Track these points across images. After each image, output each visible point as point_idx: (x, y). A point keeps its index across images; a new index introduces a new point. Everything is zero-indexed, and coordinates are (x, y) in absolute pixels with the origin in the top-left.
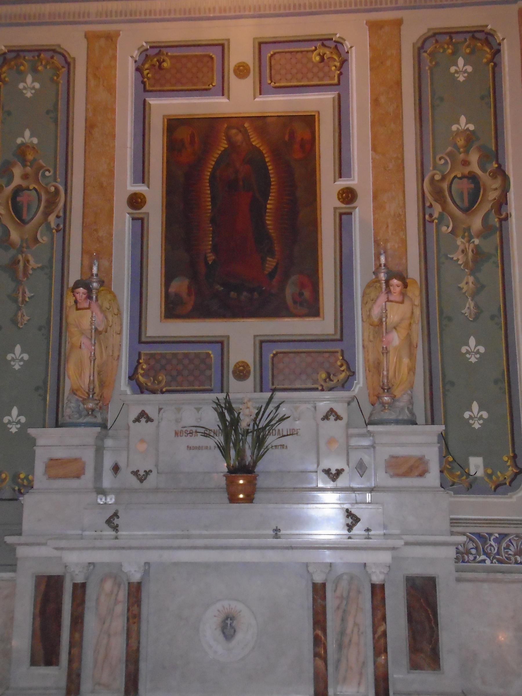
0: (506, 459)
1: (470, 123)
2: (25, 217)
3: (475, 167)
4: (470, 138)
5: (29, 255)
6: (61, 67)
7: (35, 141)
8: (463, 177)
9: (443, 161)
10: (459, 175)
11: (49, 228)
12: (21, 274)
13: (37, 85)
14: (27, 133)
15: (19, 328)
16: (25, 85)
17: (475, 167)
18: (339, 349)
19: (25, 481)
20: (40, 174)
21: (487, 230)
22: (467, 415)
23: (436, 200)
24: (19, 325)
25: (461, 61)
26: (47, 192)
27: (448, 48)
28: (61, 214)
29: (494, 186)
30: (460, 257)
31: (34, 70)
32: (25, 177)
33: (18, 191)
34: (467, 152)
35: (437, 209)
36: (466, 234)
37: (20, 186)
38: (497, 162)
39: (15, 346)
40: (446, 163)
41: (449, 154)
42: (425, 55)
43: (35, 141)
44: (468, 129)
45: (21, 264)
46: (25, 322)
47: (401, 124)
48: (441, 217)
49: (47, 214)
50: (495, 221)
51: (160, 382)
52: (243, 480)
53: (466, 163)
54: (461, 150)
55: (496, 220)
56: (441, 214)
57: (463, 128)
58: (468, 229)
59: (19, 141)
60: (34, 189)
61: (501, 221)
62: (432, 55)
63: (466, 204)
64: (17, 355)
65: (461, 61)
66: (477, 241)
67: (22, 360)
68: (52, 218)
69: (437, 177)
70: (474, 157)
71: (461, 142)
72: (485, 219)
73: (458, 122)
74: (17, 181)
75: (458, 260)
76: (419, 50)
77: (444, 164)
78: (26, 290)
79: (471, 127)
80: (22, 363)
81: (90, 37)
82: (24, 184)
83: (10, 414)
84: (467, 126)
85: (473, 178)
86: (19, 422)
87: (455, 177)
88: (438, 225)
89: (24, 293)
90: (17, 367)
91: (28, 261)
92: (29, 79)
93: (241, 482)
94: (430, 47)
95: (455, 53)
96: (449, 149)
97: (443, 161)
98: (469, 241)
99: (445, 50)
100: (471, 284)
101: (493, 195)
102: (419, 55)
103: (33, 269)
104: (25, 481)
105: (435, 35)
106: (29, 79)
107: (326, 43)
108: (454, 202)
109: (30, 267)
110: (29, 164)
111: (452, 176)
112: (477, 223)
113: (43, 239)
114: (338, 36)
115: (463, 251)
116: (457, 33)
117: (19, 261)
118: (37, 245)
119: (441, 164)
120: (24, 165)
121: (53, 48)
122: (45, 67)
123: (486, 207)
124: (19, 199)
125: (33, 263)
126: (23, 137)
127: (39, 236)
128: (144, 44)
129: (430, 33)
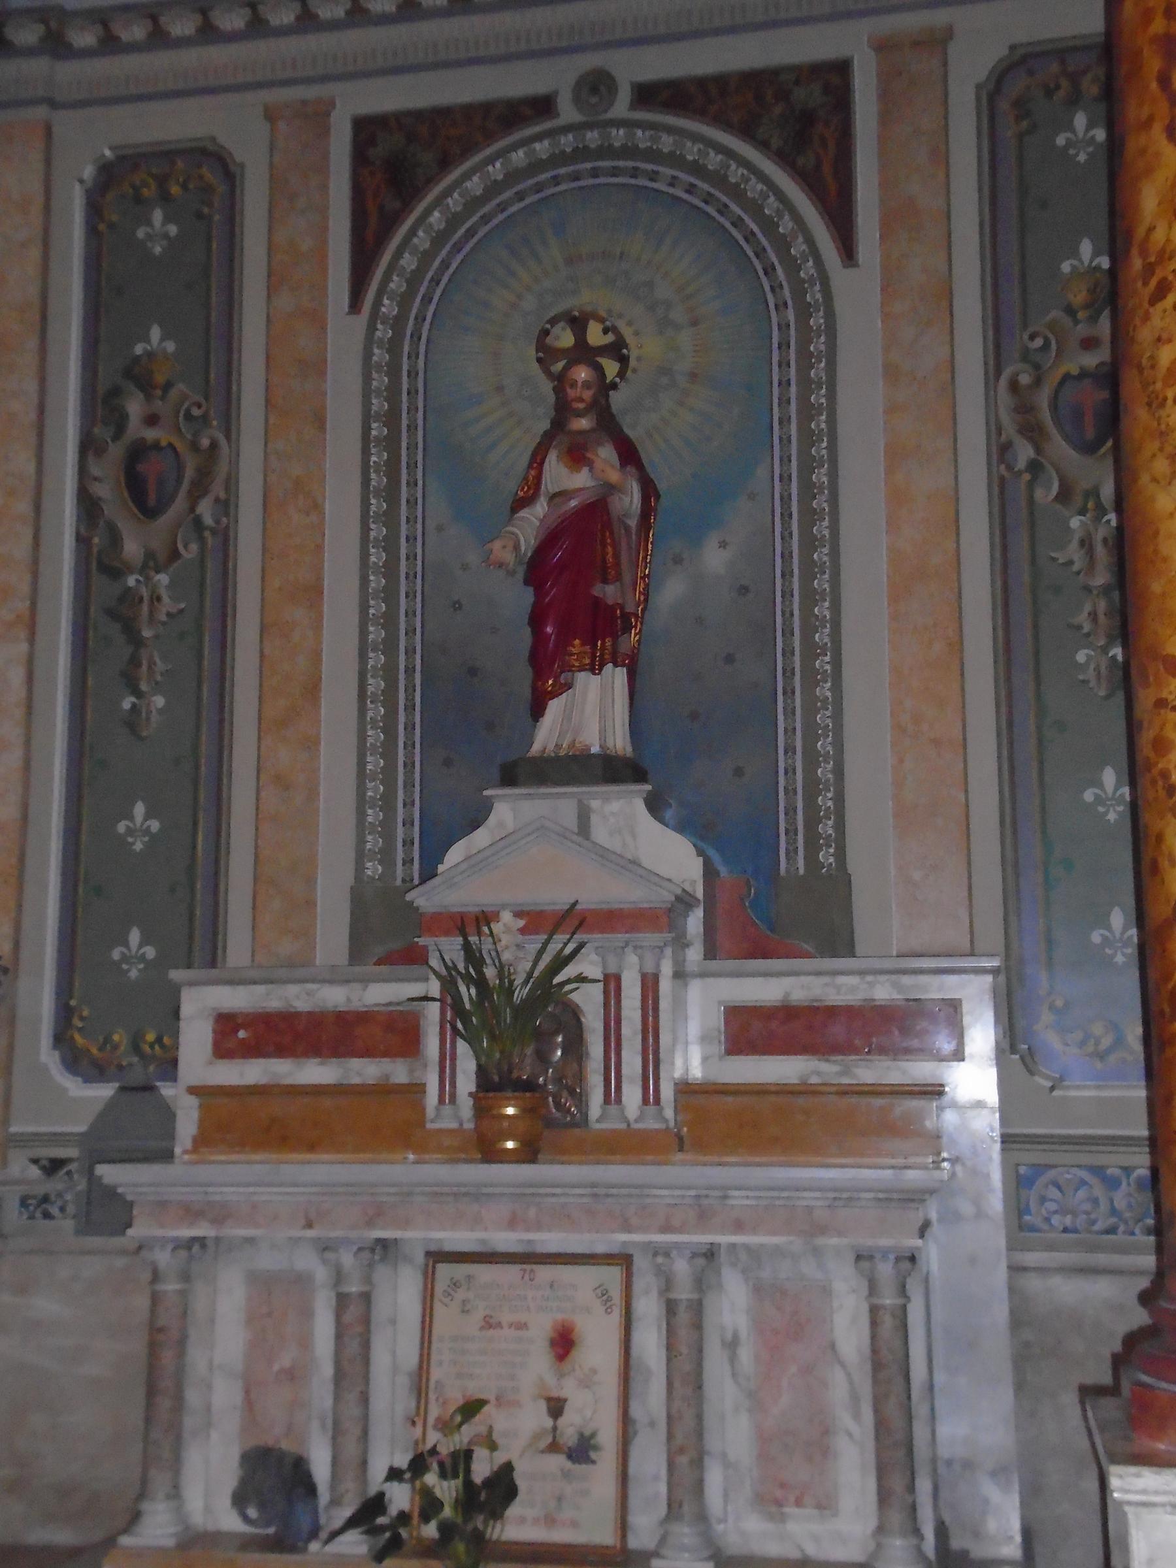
2: (152, 501)
5: (156, 654)
6: (192, 516)
7: (170, 346)
9: (1039, 342)
10: (1075, 371)
11: (198, 523)
13: (173, 230)
14: (155, 333)
16: (149, 230)
18: (554, 77)
19: (157, 1047)
25: (1080, 120)
26: (194, 446)
28: (222, 495)
30: (1076, 558)
31: (165, 198)
32: (152, 420)
35: (1024, 453)
36: (1090, 505)
39: (128, 933)
40: (1046, 346)
43: (170, 346)
48: (1035, 467)
51: (116, 1047)
54: (1081, 315)
59: (139, 349)
60: (170, 445)
65: (1080, 120)
67: (166, 236)
68: (205, 509)
69: (1025, 379)
73: (1075, 253)
75: (1071, 563)
76: (993, 91)
82: (151, 434)
86: (147, 831)
88: (1031, 485)
89: (152, 664)
91: (159, 599)
92: (158, 216)
93: (510, 1111)
94: (1017, 85)
97: (1039, 342)
98: (1097, 519)
100: (1102, 619)
103: (168, 614)
104: (157, 1047)
106: (158, 216)
110: (159, 392)
113: (190, 552)
115: (1082, 543)
116: (1075, 49)
119: (1036, 350)
120: (149, 397)
122: (184, 187)
124: (140, 467)
125: (168, 604)
126: (148, 342)
127: (180, 547)
128: (108, 153)
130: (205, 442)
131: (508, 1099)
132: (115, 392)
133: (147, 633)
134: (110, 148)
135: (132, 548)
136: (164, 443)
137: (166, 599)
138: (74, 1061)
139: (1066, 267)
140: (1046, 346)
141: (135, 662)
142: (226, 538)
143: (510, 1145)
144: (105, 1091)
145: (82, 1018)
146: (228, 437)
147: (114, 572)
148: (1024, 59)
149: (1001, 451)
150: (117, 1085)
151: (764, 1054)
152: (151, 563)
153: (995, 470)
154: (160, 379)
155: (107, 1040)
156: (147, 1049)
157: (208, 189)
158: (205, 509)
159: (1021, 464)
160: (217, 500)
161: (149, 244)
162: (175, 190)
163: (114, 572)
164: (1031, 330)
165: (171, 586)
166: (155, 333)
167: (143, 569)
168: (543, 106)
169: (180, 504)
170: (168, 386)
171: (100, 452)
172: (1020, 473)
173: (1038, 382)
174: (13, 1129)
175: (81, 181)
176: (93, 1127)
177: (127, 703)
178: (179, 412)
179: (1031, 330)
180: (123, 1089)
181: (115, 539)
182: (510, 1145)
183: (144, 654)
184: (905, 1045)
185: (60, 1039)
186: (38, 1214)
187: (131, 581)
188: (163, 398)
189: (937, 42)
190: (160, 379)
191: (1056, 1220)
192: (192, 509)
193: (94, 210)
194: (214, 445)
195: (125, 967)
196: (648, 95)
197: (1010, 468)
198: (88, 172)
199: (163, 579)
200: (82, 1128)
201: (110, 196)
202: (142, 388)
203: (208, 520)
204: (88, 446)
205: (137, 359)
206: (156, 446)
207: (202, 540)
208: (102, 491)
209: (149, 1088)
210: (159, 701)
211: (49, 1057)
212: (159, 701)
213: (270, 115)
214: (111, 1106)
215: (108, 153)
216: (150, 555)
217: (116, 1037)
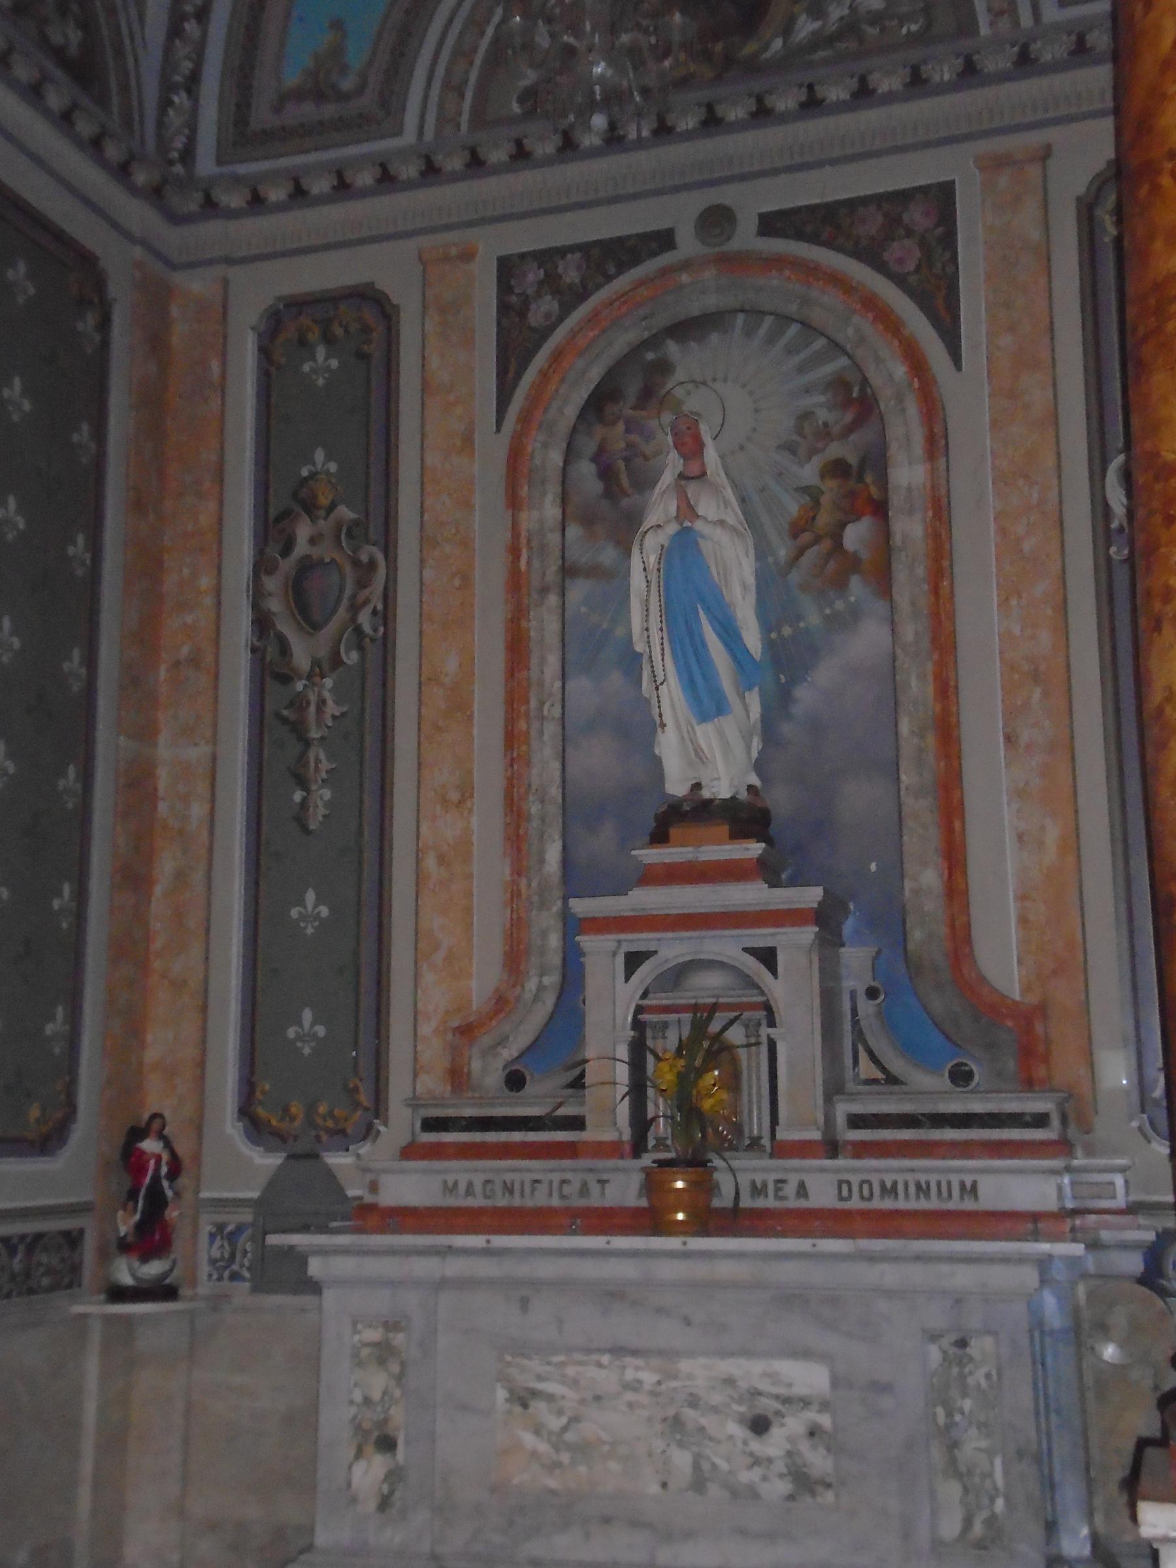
7: (333, 467)
11: (358, 630)
13: (334, 363)
18: (680, 214)
20: (343, 537)
26: (356, 563)
28: (380, 607)
31: (328, 339)
32: (313, 541)
33: (307, 566)
37: (308, 557)
39: (302, 1011)
45: (312, 709)
46: (324, 775)
47: (852, 204)
49: (355, 609)
52: (684, 1212)
60: (333, 560)
64: (319, 467)
67: (328, 369)
68: (364, 618)
74: (302, 548)
78: (322, 756)
80: (313, 1044)
83: (301, 902)
90: (310, 931)
91: (324, 702)
92: (321, 352)
93: (680, 1184)
103: (334, 717)
106: (321, 352)
110: (322, 513)
117: (308, 703)
118: (341, 669)
125: (332, 708)
130: (364, 558)
131: (678, 1173)
132: (286, 515)
133: (314, 734)
135: (301, 658)
136: (327, 560)
137: (330, 703)
138: (257, 1128)
141: (302, 758)
142: (387, 645)
143: (680, 1216)
144: (274, 1160)
146: (386, 557)
150: (285, 1155)
151: (877, 1128)
152: (317, 670)
154: (324, 501)
155: (286, 1110)
156: (319, 1121)
157: (366, 330)
158: (364, 618)
160: (375, 612)
161: (314, 377)
163: (285, 679)
167: (310, 677)
168: (664, 240)
169: (342, 613)
170: (332, 507)
171: (271, 570)
174: (204, 1194)
177: (298, 796)
178: (340, 530)
180: (289, 1157)
181: (284, 649)
182: (680, 1216)
183: (311, 755)
185: (246, 1112)
187: (299, 686)
188: (325, 519)
190: (324, 501)
192: (354, 619)
193: (264, 351)
194: (372, 565)
195: (299, 1044)
196: (770, 224)
199: (328, 682)
200: (255, 1194)
202: (309, 512)
203: (367, 628)
204: (262, 566)
207: (361, 648)
208: (275, 605)
209: (314, 1156)
210: (327, 794)
211: (232, 1129)
212: (327, 794)
214: (281, 1168)
216: (316, 663)
217: (294, 1110)
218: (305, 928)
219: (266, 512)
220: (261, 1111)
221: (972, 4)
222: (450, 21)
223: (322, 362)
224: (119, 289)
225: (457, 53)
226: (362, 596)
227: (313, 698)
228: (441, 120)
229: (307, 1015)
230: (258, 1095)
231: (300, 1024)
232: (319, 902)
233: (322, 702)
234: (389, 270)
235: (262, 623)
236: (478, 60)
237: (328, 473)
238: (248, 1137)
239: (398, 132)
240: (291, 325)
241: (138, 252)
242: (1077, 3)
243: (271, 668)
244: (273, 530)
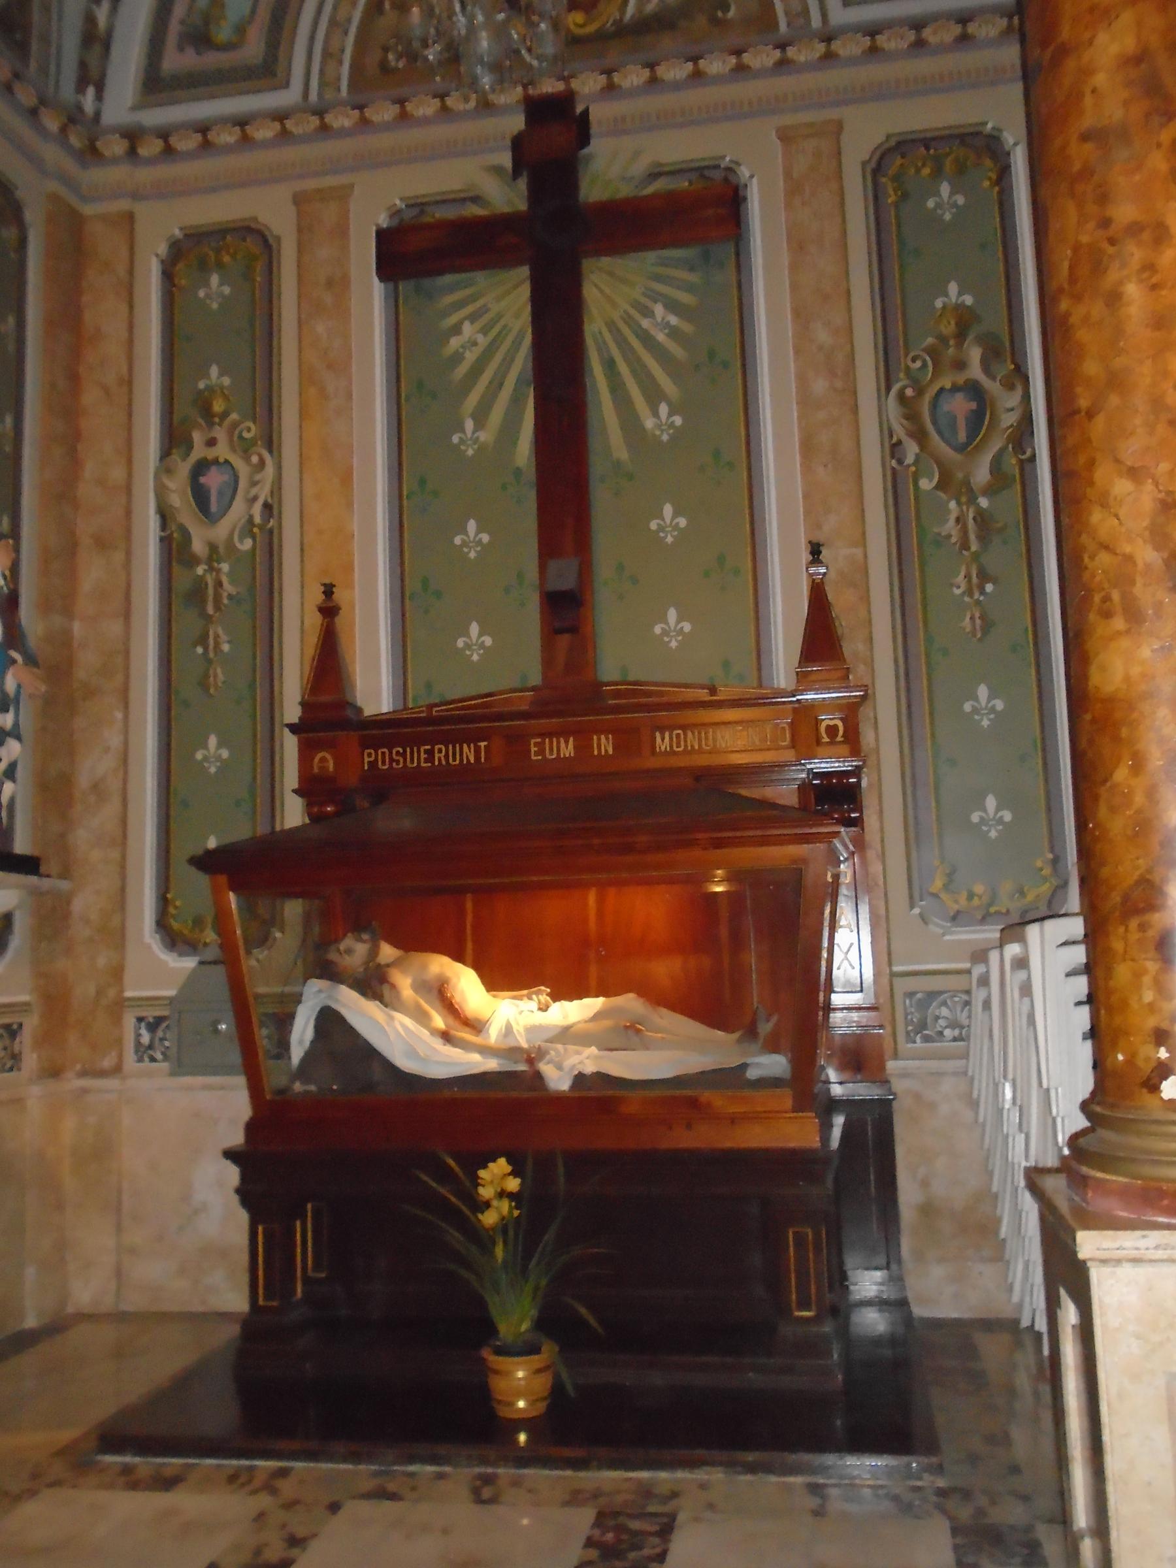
0: (1039, 864)
1: (957, 193)
2: (214, 508)
3: (975, 371)
4: (965, 320)
7: (226, 381)
8: (955, 389)
9: (918, 364)
12: (210, 610)
14: (214, 371)
15: (211, 696)
17: (975, 371)
21: (999, 481)
22: (967, 707)
23: (911, 435)
24: (212, 691)
27: (924, 165)
29: (1009, 405)
30: (954, 533)
34: (960, 344)
35: (912, 449)
38: (1013, 362)
40: (925, 365)
41: (932, 352)
42: (884, 180)
43: (226, 381)
44: (963, 305)
50: (1011, 462)
53: (960, 365)
55: (1014, 461)
56: (917, 461)
57: (954, 301)
58: (966, 483)
59: (201, 385)
61: (1021, 462)
62: (896, 178)
63: (962, 436)
65: (945, 189)
66: (984, 502)
69: (909, 392)
70: (975, 354)
71: (948, 328)
72: (996, 466)
76: (877, 169)
77: (920, 369)
79: (968, 300)
81: (299, 200)
82: (211, 453)
83: (205, 746)
84: (961, 299)
85: (974, 390)
87: (942, 390)
89: (215, 676)
95: (938, 173)
96: (930, 340)
97: (918, 364)
99: (918, 171)
101: (1009, 420)
102: (876, 184)
103: (230, 597)
105: (900, 147)
106: (215, 279)
107: (706, 173)
108: (939, 432)
109: (225, 594)
110: (217, 420)
111: (936, 388)
112: (982, 475)
114: (728, 159)
115: (958, 520)
121: (247, 223)
122: (233, 256)
123: (996, 445)
125: (228, 588)
128: (398, 202)
129: (892, 143)
134: (401, 199)
136: (221, 460)
138: (173, 940)
139: (939, 304)
140: (925, 365)
145: (176, 907)
147: (191, 561)
148: (899, 144)
149: (895, 449)
153: (888, 464)
159: (910, 459)
161: (208, 301)
162: (226, 259)
164: (912, 354)
165: (230, 574)
166: (214, 371)
170: (225, 415)
172: (909, 466)
173: (920, 392)
175: (157, 255)
176: (182, 990)
179: (912, 354)
180: (201, 963)
184: (323, 995)
185: (162, 924)
186: (146, 1059)
187: (200, 570)
188: (220, 425)
189: (342, 195)
191: (948, 1033)
193: (168, 275)
197: (900, 462)
198: (163, 249)
199: (225, 567)
200: (171, 993)
201: (180, 266)
205: (200, 392)
206: (216, 462)
208: (175, 500)
213: (786, 137)
214: (194, 970)
215: (398, 202)
218: (943, 215)
219: (171, 419)
220: (175, 925)
221: (772, 5)
222: (312, 38)
223: (216, 288)
224: (35, 217)
225: (327, 54)
226: (254, 491)
227: (210, 579)
228: (323, 84)
229: (213, 741)
230: (172, 910)
231: (206, 747)
232: (220, 745)
233: (219, 584)
234: (273, 210)
235: (165, 515)
236: (353, 30)
237: (222, 388)
238: (166, 947)
239: (286, 85)
240: (190, 253)
241: (53, 186)
242: (859, 4)
243: (175, 550)
244: (174, 439)
